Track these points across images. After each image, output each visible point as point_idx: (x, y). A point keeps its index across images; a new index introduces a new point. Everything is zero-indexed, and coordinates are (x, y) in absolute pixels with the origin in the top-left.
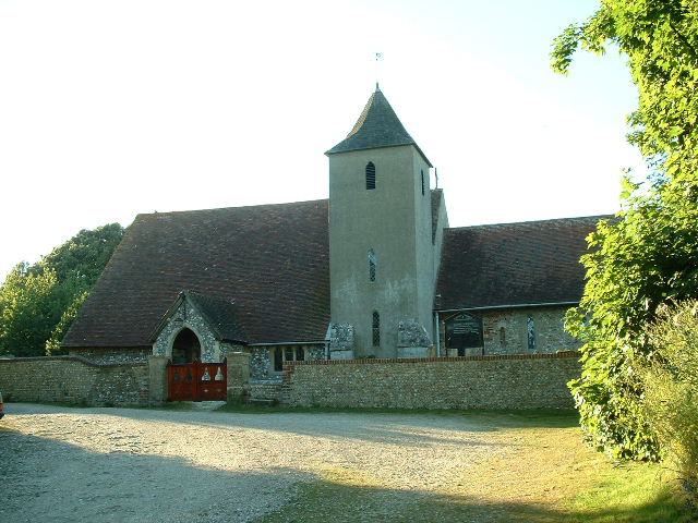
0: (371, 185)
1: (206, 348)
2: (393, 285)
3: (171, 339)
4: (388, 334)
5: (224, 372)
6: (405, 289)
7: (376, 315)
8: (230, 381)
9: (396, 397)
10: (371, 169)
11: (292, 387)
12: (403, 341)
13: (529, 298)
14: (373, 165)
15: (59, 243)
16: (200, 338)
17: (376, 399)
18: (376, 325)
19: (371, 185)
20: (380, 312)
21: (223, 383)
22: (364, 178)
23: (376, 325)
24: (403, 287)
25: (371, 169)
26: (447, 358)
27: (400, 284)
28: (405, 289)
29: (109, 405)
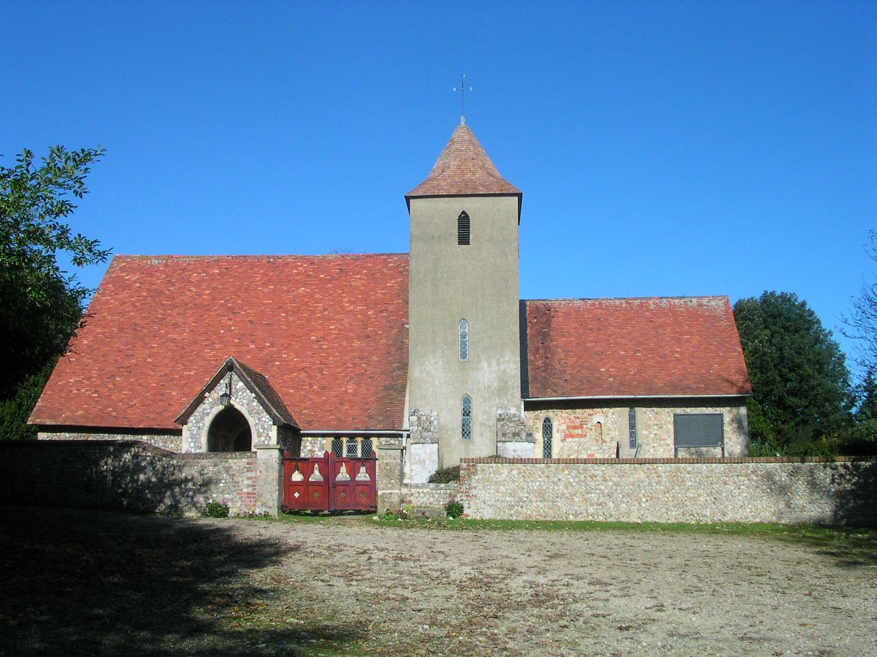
0: (464, 239)
1: (259, 436)
2: (489, 366)
3: (208, 420)
4: (482, 424)
5: (371, 471)
6: (505, 371)
7: (467, 401)
8: (380, 483)
9: (617, 507)
10: (464, 220)
11: (474, 492)
12: (504, 435)
13: (264, 393)
14: (467, 216)
15: (819, 314)
16: (252, 421)
17: (591, 510)
18: (467, 413)
19: (464, 239)
20: (473, 397)
21: (371, 487)
22: (455, 231)
23: (467, 413)
24: (502, 367)
25: (464, 220)
26: (676, 460)
27: (498, 364)
28: (505, 371)
29: (315, 514)
